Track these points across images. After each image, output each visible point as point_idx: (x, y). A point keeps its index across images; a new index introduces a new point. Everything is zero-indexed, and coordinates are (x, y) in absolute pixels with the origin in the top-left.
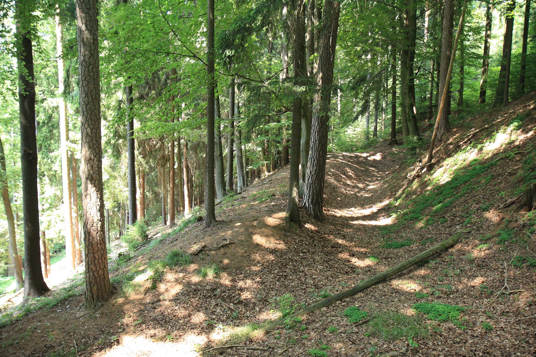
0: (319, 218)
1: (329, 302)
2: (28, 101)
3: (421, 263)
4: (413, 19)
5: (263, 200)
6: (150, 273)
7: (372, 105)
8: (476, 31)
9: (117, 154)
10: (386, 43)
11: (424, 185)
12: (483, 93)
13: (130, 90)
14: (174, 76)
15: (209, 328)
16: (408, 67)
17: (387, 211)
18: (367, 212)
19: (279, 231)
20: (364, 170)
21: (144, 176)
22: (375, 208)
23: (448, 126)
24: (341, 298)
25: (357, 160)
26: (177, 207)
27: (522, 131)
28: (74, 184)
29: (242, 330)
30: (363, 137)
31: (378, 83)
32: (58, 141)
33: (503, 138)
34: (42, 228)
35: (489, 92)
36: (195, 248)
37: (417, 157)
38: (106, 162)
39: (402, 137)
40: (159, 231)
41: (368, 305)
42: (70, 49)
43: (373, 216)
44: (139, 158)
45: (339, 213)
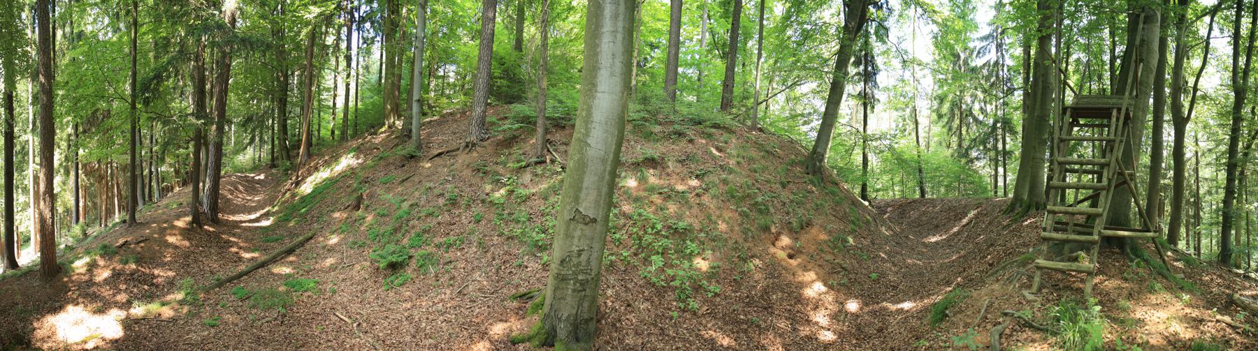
0: (215, 221)
1: (220, 284)
2: (10, 137)
3: (290, 252)
4: (286, 77)
5: (172, 209)
6: (87, 259)
7: (257, 139)
8: (328, 90)
9: (67, 173)
10: (267, 93)
11: (293, 196)
12: (333, 132)
13: (76, 127)
14: (108, 114)
15: (127, 305)
16: (283, 111)
17: (267, 215)
18: (253, 216)
19: (186, 233)
20: (251, 186)
21: (86, 189)
22: (258, 215)
23: (309, 155)
24: (230, 280)
25: (246, 179)
26: (110, 213)
27: (1104, 90)
28: (36, 193)
29: (154, 307)
30: (251, 164)
31: (261, 122)
32: (28, 163)
33: (347, 162)
34: (16, 223)
35: (337, 132)
36: (121, 241)
37: (288, 176)
38: (57, 180)
39: (279, 162)
40: (94, 230)
41: (251, 285)
42: (35, 98)
43: (257, 220)
44: (82, 176)
45: (232, 218)
